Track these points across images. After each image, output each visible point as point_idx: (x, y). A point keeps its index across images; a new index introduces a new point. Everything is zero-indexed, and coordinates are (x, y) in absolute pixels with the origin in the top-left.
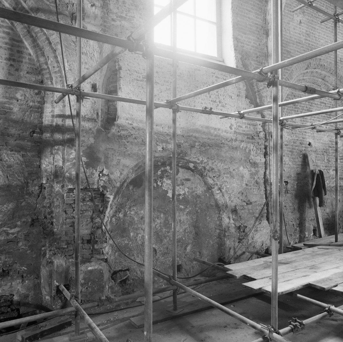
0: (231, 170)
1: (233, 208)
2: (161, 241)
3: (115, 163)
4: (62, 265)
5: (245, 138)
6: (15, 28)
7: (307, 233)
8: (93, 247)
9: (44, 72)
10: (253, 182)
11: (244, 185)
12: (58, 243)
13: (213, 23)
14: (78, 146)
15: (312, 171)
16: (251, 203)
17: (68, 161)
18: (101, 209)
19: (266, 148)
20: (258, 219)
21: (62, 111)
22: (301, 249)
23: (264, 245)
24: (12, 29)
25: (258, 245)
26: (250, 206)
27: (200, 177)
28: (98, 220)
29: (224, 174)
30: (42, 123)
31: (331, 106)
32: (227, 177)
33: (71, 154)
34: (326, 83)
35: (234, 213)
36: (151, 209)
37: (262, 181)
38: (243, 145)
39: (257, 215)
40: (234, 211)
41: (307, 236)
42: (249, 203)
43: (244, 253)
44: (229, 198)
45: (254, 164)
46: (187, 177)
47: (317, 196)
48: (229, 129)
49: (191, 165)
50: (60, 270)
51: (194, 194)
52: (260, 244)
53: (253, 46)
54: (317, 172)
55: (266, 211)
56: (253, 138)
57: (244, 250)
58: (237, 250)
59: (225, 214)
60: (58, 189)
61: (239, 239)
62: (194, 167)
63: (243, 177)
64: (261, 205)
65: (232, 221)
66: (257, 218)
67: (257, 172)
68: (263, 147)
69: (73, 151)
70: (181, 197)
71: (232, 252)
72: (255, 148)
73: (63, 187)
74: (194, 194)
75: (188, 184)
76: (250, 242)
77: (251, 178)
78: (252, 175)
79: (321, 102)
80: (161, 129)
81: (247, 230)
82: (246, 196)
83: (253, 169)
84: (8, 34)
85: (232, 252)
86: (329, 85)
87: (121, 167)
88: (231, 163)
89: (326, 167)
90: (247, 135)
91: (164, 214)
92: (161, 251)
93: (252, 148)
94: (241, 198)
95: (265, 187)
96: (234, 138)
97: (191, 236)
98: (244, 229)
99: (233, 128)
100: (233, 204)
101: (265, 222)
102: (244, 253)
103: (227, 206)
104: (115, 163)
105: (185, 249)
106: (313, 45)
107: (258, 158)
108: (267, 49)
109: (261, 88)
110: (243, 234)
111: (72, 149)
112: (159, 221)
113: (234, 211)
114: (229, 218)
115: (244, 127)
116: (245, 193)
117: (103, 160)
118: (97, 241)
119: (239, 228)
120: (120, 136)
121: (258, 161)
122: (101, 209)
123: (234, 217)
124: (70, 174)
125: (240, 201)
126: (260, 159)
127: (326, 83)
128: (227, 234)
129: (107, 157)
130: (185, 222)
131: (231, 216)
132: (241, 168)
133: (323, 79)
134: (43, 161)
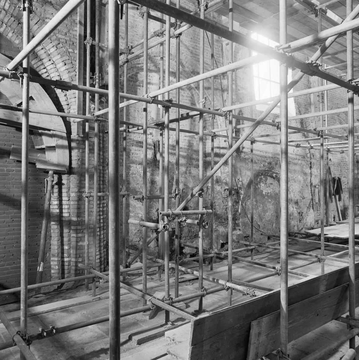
0: (295, 177)
1: (296, 201)
2: (262, 220)
3: (244, 174)
4: (224, 231)
5: (300, 158)
6: (194, 97)
7: (330, 219)
8: (235, 222)
9: (207, 122)
10: (305, 185)
11: (301, 187)
12: (221, 220)
13: (278, 83)
14: (99, 150)
15: (334, 178)
16: (305, 198)
17: (224, 173)
18: (237, 201)
19: (311, 164)
20: (308, 208)
21: (219, 145)
22: (335, 225)
23: (312, 224)
24: (192, 98)
25: (309, 224)
26: (304, 200)
27: (277, 182)
28: (237, 207)
29: (291, 180)
30: (206, 151)
31: (342, 133)
32: (293, 182)
33: (226, 169)
34: (340, 118)
35: (296, 204)
36: (146, 209)
37: (309, 185)
38: (300, 162)
39: (308, 206)
40: (297, 203)
41: (330, 221)
42: (304, 198)
43: (302, 229)
44: (294, 195)
45: (305, 174)
46: (271, 182)
47: (337, 194)
48: (293, 152)
49: (274, 175)
50: (224, 234)
51: (275, 192)
52: (310, 224)
53: (303, 99)
54: (337, 179)
55: (312, 203)
56: (304, 157)
57: (302, 227)
58: (299, 227)
59: (290, 205)
60: (219, 189)
61: (300, 220)
62: (276, 176)
63: (300, 182)
64: (309, 199)
65: (295, 209)
66: (308, 207)
67: (307, 179)
68: (309, 163)
69: (227, 168)
70: (269, 194)
71: (296, 228)
72: (305, 164)
73: (222, 188)
74: (275, 192)
75: (272, 186)
76: (305, 222)
77: (304, 182)
78: (305, 180)
79: (336, 131)
80: (262, 154)
81: (303, 215)
82: (302, 194)
83: (305, 177)
84: (190, 100)
85: (296, 228)
86: (341, 119)
87: (247, 177)
88: (294, 173)
89: (340, 175)
90: (302, 155)
91: (262, 204)
92: (262, 226)
93: (304, 164)
94: (300, 195)
95: (311, 189)
96: (295, 158)
97: (275, 218)
98: (302, 214)
99: (295, 151)
100: (296, 199)
101: (312, 210)
102: (302, 229)
103: (292, 200)
104: (244, 174)
105: (273, 226)
106: (333, 95)
107: (307, 170)
108: (310, 100)
109: (307, 125)
110: (301, 217)
111: (226, 166)
112: (260, 209)
113: (297, 203)
114: (293, 207)
115: (300, 151)
116: (301, 192)
117: (239, 173)
118: (237, 219)
119: (299, 213)
120: (245, 159)
121: (307, 172)
122: (237, 201)
123: (296, 206)
124: (226, 180)
125: (299, 197)
126: (308, 171)
127: (340, 118)
128: (291, 218)
129: (241, 171)
130: (272, 209)
131: (294, 206)
132: (299, 177)
133: (338, 116)
134: (207, 173)
